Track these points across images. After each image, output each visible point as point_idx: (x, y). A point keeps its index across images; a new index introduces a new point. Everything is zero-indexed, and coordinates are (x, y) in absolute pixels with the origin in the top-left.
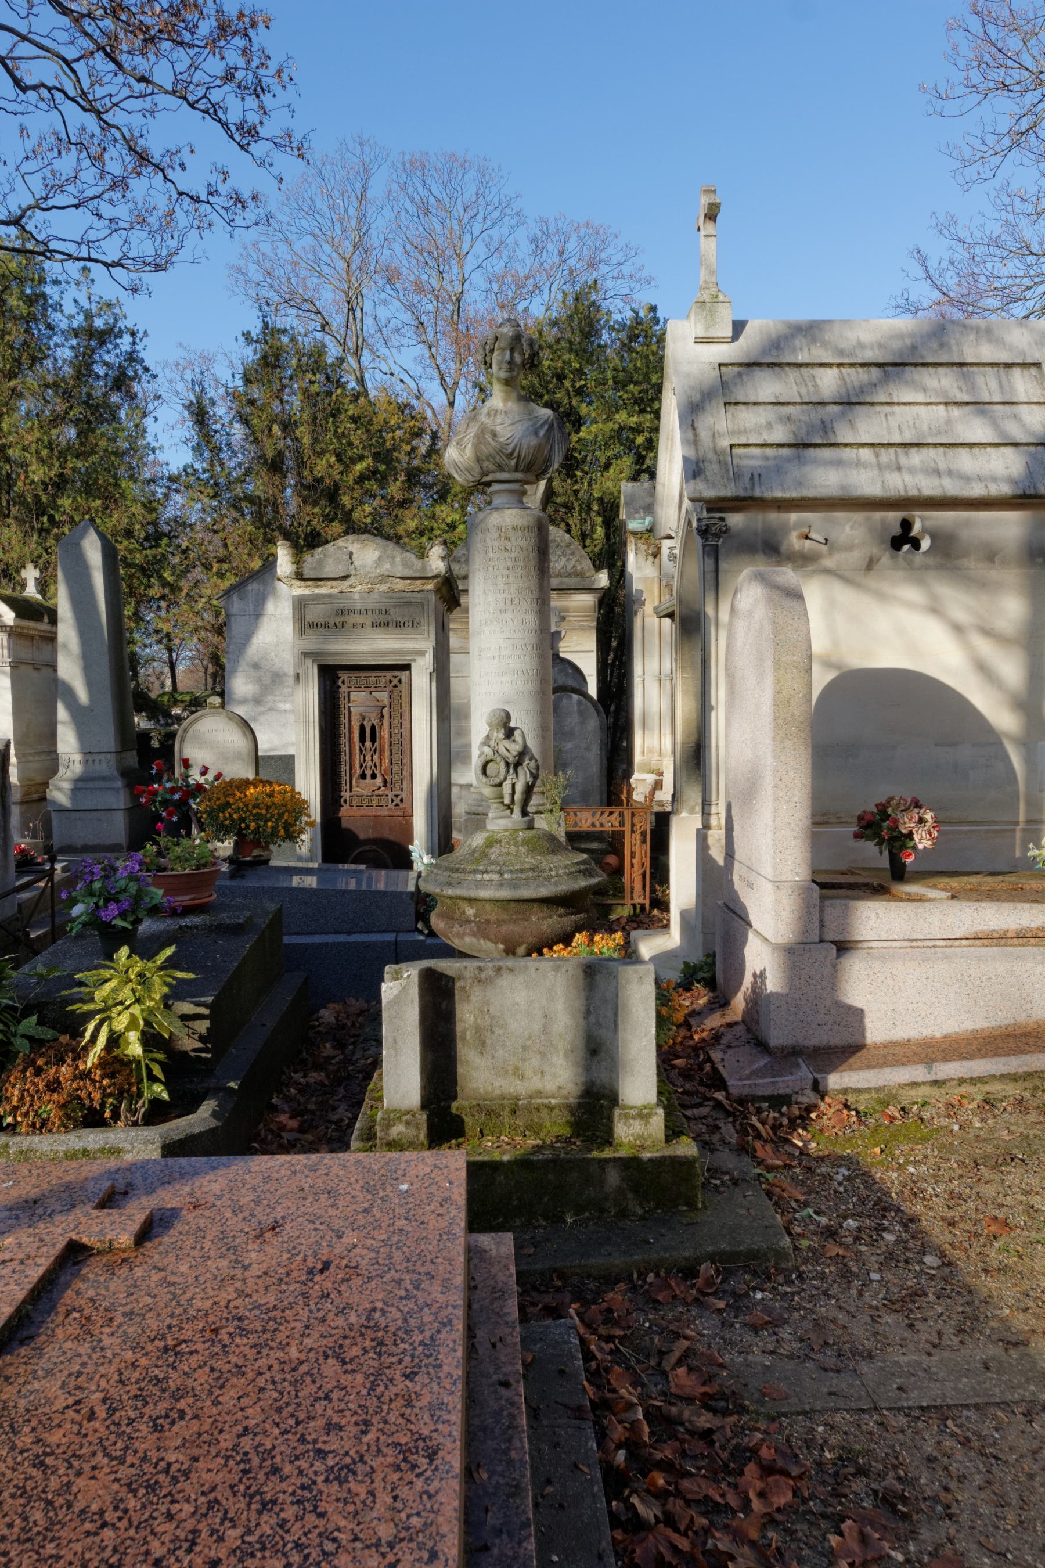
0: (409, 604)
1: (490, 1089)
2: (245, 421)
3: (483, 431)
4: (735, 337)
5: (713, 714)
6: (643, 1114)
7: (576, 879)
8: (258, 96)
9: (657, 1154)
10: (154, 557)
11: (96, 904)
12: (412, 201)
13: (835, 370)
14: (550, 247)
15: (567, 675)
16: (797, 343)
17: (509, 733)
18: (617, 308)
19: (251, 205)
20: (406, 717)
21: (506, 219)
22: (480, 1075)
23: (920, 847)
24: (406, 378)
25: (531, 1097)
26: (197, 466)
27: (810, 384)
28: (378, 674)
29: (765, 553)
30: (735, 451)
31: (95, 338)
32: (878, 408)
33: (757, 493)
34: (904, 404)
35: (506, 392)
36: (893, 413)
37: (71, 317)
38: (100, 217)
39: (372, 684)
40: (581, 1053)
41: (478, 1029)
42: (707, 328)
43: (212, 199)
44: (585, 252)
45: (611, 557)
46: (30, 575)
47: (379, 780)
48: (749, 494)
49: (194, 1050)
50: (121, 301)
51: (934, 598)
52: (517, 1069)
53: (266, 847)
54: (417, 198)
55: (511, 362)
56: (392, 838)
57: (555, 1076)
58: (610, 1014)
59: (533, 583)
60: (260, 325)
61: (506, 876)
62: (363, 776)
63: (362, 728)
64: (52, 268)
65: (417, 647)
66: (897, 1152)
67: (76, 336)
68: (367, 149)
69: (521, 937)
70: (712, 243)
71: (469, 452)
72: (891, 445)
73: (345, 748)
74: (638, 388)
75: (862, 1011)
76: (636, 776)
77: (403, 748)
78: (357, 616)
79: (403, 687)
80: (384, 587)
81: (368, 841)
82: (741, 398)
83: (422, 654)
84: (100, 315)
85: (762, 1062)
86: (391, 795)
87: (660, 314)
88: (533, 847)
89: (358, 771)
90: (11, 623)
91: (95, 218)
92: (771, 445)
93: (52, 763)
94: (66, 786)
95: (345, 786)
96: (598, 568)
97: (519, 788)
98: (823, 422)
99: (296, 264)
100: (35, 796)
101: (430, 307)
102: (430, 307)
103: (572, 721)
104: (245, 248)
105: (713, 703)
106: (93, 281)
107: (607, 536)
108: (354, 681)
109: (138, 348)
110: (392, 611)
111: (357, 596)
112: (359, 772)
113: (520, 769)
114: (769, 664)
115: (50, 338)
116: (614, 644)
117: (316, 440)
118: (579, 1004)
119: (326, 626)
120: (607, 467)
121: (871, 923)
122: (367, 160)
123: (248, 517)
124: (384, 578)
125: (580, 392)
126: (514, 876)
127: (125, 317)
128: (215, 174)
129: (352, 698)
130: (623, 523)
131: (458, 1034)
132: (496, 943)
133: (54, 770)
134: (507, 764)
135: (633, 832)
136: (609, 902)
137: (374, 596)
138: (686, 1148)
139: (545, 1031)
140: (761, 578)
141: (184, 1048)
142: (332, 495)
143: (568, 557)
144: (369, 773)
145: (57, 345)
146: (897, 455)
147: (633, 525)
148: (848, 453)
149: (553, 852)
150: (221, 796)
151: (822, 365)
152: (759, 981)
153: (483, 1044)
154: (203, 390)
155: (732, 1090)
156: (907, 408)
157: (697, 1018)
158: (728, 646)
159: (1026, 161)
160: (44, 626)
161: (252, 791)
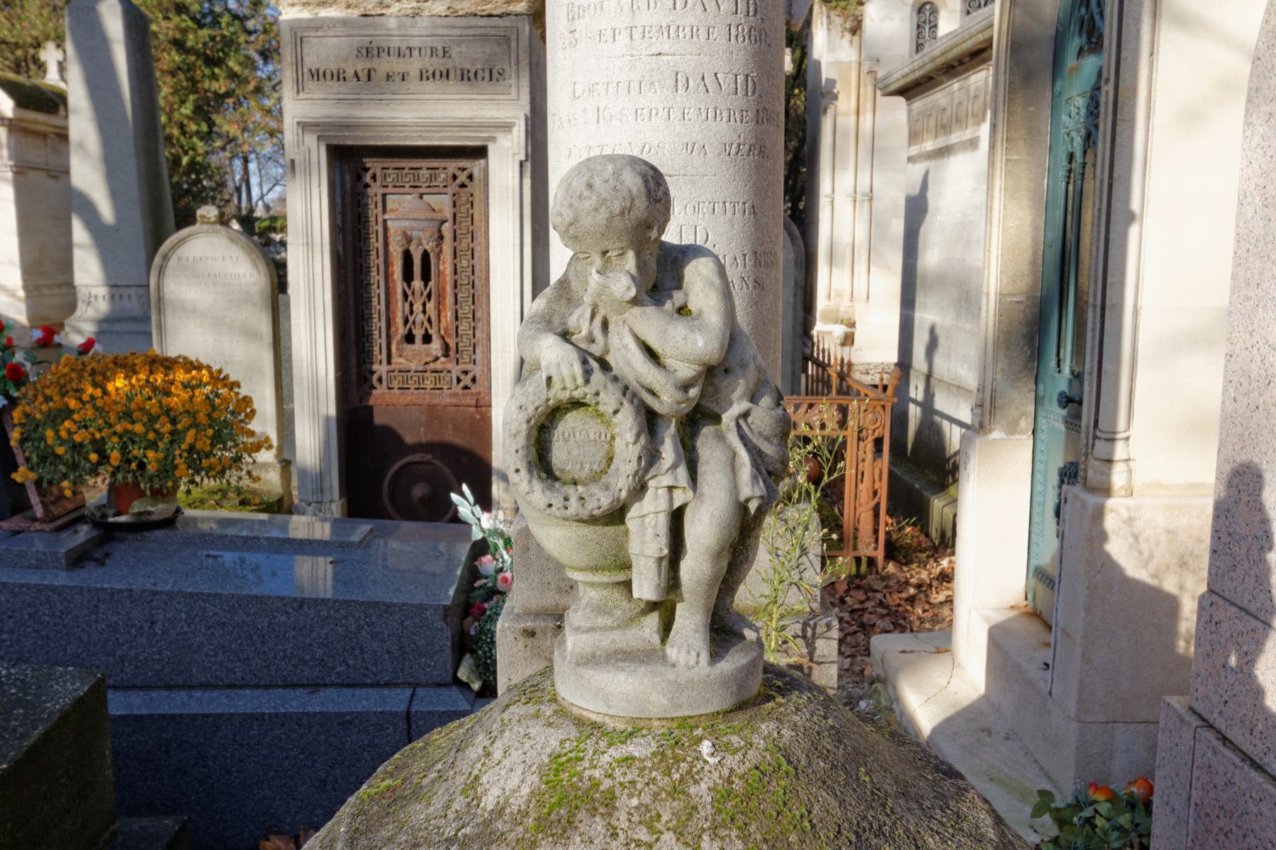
5: (1133, 231)
17: (662, 274)
20: (480, 238)
39: (423, 182)
47: (436, 346)
56: (457, 441)
63: (407, 257)
78: (394, 59)
79: (475, 187)
83: (507, 127)
86: (456, 371)
89: (401, 331)
93: (69, 300)
95: (379, 354)
97: (704, 531)
105: (1135, 205)
110: (454, 52)
111: (392, 23)
119: (339, 76)
129: (390, 205)
133: (71, 307)
134: (650, 421)
137: (423, 23)
161: (120, 382)
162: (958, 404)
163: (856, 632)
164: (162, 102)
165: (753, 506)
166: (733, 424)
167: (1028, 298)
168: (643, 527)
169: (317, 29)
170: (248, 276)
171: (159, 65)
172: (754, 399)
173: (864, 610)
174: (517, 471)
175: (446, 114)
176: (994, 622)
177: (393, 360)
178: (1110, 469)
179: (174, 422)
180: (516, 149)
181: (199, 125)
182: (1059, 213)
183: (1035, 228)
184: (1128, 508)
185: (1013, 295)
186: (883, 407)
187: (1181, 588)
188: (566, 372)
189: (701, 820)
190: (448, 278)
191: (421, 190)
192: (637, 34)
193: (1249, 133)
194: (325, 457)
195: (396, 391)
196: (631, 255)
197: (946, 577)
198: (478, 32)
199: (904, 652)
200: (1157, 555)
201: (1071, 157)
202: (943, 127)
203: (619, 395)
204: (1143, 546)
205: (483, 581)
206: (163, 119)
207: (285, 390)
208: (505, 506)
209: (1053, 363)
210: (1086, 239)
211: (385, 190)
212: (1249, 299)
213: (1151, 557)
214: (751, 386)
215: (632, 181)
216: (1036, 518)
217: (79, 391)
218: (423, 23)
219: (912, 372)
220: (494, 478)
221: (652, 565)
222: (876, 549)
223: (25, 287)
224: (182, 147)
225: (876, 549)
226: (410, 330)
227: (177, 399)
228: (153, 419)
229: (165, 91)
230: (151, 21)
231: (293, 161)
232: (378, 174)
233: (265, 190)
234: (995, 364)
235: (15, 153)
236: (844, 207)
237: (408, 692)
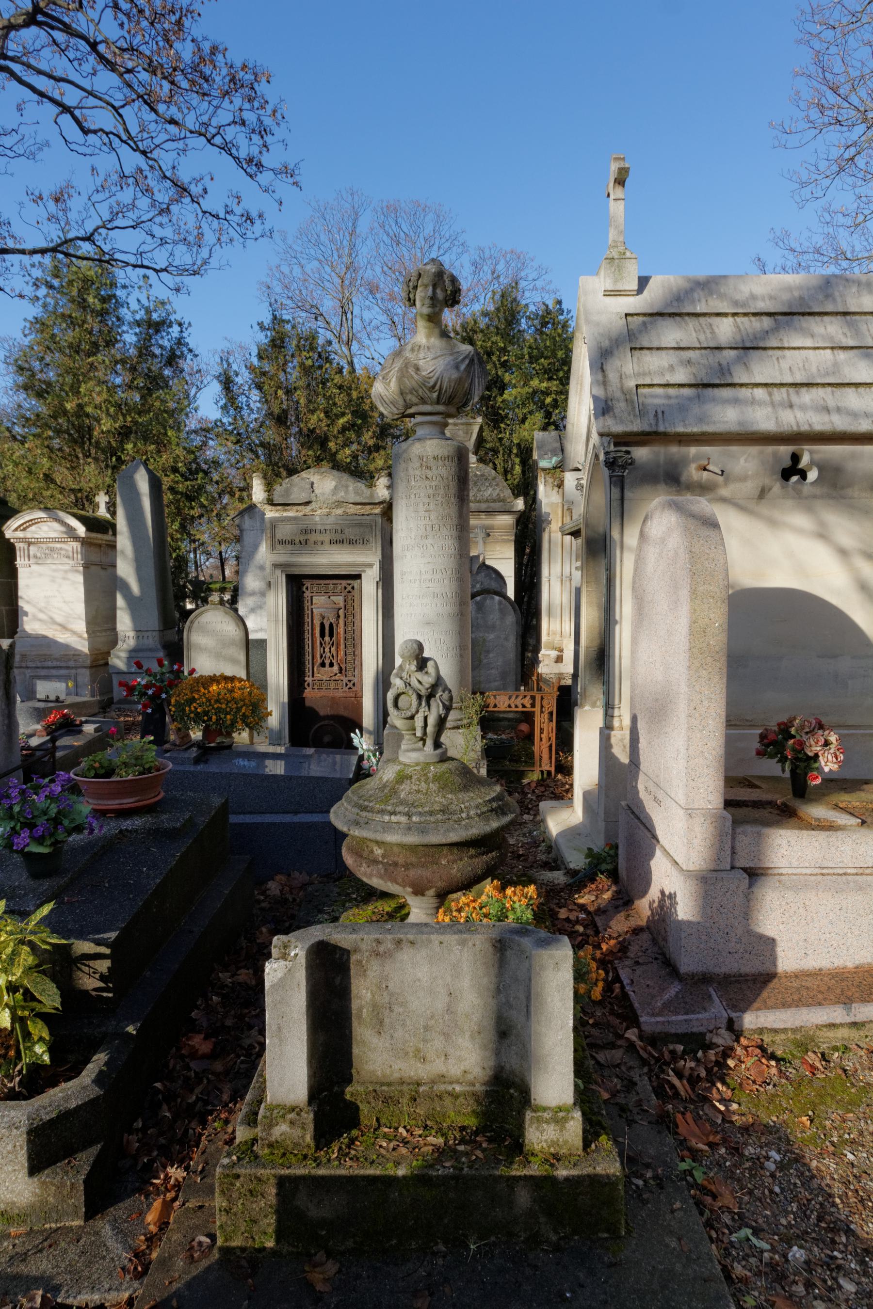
0: (360, 525)
1: (388, 1072)
2: (259, 387)
3: (406, 366)
4: (640, 290)
5: (617, 628)
6: (558, 1116)
7: (487, 819)
8: (262, 137)
9: (575, 1172)
10: (193, 486)
11: (13, 829)
12: (388, 235)
13: (730, 319)
14: (485, 268)
15: (491, 578)
16: (696, 295)
18: (532, 300)
19: (258, 222)
20: (357, 617)
21: (454, 248)
22: (376, 1056)
23: (826, 769)
25: (433, 1082)
26: (225, 420)
27: (708, 331)
29: (666, 484)
30: (641, 391)
31: (154, 326)
32: (770, 352)
33: (661, 429)
34: (794, 348)
35: (429, 328)
36: (784, 357)
37: (134, 312)
38: (153, 236)
40: (490, 1035)
41: (375, 1006)
42: (616, 281)
44: (510, 272)
45: (526, 487)
46: (102, 499)
47: (336, 668)
48: (654, 429)
49: (95, 990)
51: (822, 524)
52: (418, 1050)
53: (229, 735)
54: (391, 233)
55: (433, 298)
57: (460, 1059)
58: (522, 996)
59: (453, 510)
60: (270, 317)
61: (414, 819)
62: (323, 665)
63: (322, 626)
64: (121, 275)
65: (367, 560)
66: (828, 1123)
67: (139, 326)
68: (356, 197)
69: (429, 882)
70: (621, 205)
71: (393, 385)
72: (782, 385)
73: (308, 642)
74: (547, 361)
75: (774, 940)
76: (543, 652)
79: (355, 593)
80: (339, 511)
81: (327, 717)
82: (646, 344)
83: (371, 566)
84: (156, 311)
85: (674, 989)
86: (345, 680)
88: (444, 785)
89: (319, 661)
90: (83, 535)
91: (149, 237)
92: (673, 385)
94: (123, 655)
96: (516, 496)
97: (431, 721)
98: (720, 365)
99: (305, 280)
100: (102, 662)
101: (400, 311)
102: (400, 311)
103: (494, 617)
105: (617, 617)
109: (185, 335)
110: (346, 531)
111: (317, 518)
113: (433, 702)
114: (684, 593)
115: (119, 326)
116: (528, 551)
117: (310, 401)
118: (487, 981)
119: (292, 543)
120: (523, 421)
121: (783, 851)
122: (356, 206)
123: (262, 457)
124: (339, 503)
126: (423, 819)
130: (536, 463)
131: (354, 1012)
132: (404, 887)
133: (114, 643)
134: (420, 697)
135: (542, 712)
136: (522, 768)
137: (332, 519)
138: (609, 1166)
139: (449, 1010)
140: (678, 508)
141: (85, 988)
142: (323, 442)
143: (488, 483)
144: (327, 662)
145: (123, 332)
146: (788, 395)
147: (543, 464)
148: (745, 393)
149: (465, 788)
150: (188, 692)
151: (718, 315)
152: (668, 902)
153: (381, 1022)
154: (229, 364)
155: (645, 1027)
156: (797, 352)
157: (603, 917)
158: (636, 570)
159: (846, 187)
160: (109, 537)
161: (215, 688)
189: (431, 780)
215: (415, 646)
217: (199, 691)
223: (87, 632)
227: (237, 694)
235: (85, 557)
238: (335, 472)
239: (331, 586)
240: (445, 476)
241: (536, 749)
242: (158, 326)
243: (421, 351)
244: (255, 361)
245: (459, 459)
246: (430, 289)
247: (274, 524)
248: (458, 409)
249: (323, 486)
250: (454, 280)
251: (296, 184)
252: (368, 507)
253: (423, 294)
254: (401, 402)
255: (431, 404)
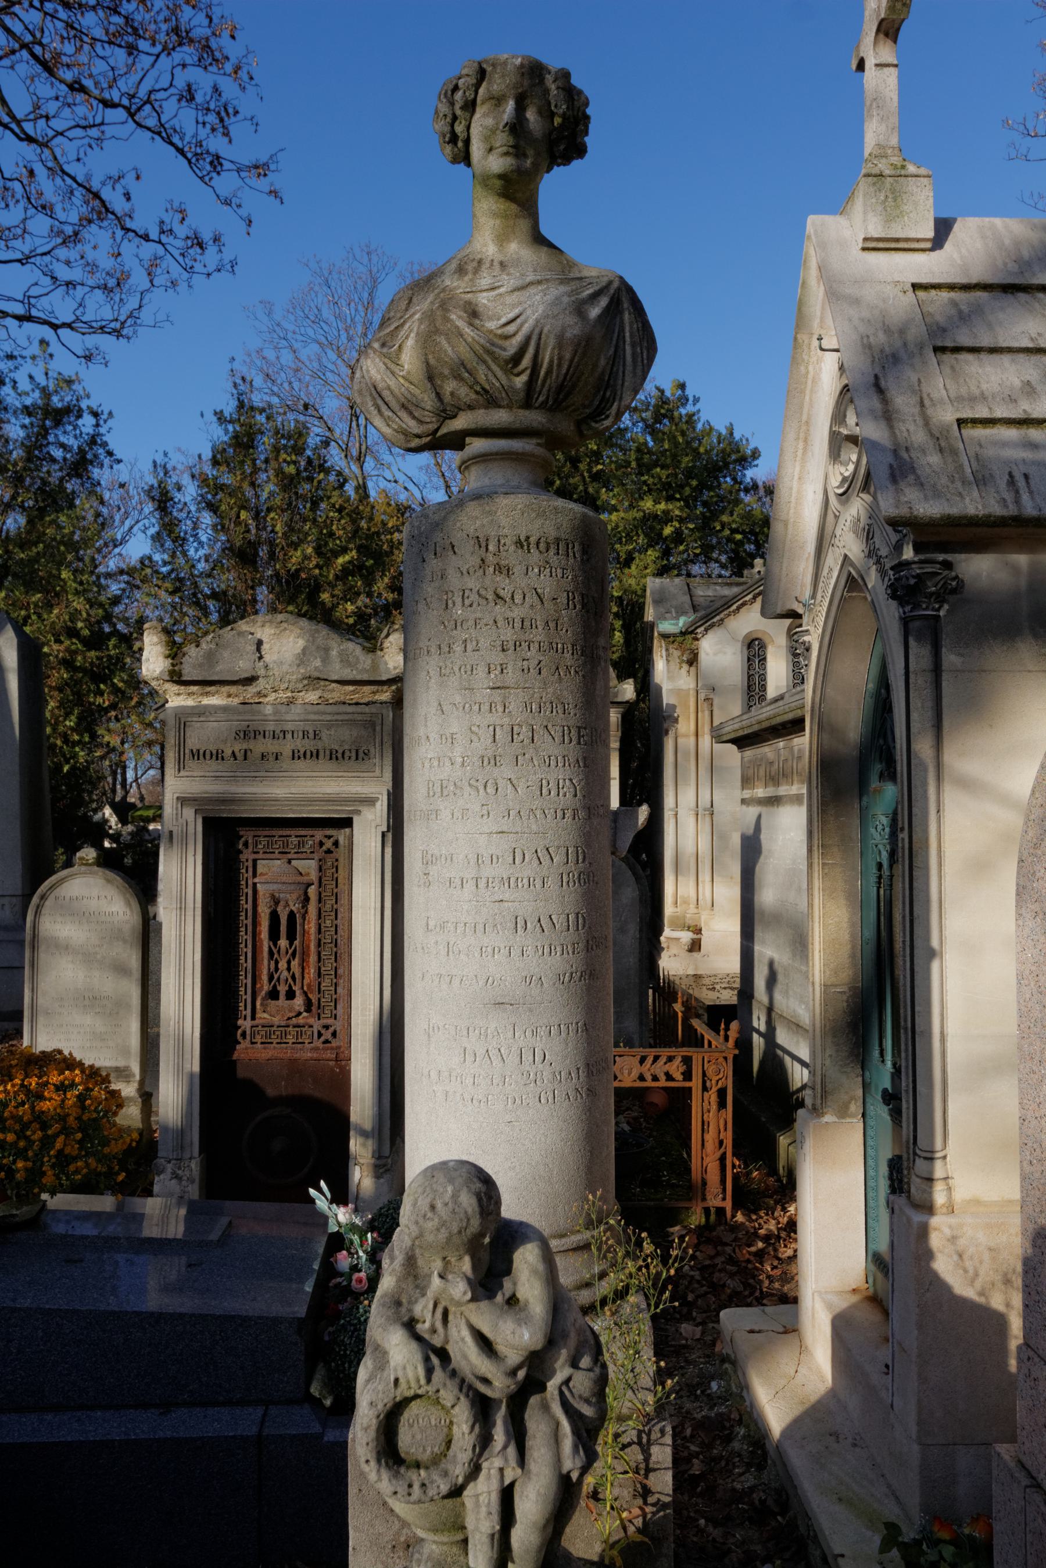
2: (212, 507)
5: (935, 966)
19: (211, 250)
20: (343, 900)
24: (411, 486)
26: (157, 557)
28: (302, 832)
30: (969, 432)
42: (889, 220)
43: (164, 239)
47: (299, 1002)
48: (1012, 510)
50: (81, 376)
55: (517, 128)
56: (317, 1094)
60: (234, 403)
62: (274, 995)
63: (274, 917)
67: (30, 414)
68: (374, 257)
71: (409, 358)
76: (667, 933)
77: (336, 949)
78: (269, 741)
80: (312, 696)
81: (280, 1100)
83: (371, 802)
87: (690, 392)
89: (266, 987)
96: (621, 678)
97: (531, 1506)
104: (249, 355)
105: (935, 943)
106: (51, 355)
107: (627, 642)
108: (264, 841)
109: (102, 430)
110: (325, 734)
111: (268, 710)
112: (266, 987)
117: (292, 530)
120: (628, 562)
122: (375, 270)
125: (596, 477)
127: (88, 396)
128: (171, 213)
129: (259, 870)
134: (483, 1408)
135: (705, 1089)
137: (297, 710)
144: (282, 989)
162: (798, 1042)
163: (706, 1293)
164: (48, 715)
165: (575, 1476)
166: (556, 1392)
167: (850, 989)
168: (477, 1504)
169: (199, 715)
170: (121, 913)
171: (49, 682)
172: (574, 1364)
173: (715, 1266)
174: (367, 1461)
175: (315, 790)
176: (838, 1310)
177: (258, 1016)
178: (931, 1187)
179: (44, 1127)
180: (378, 821)
181: (82, 735)
182: (873, 914)
183: (852, 925)
184: (950, 1227)
185: (836, 986)
186: (725, 1058)
187: (1008, 1305)
188: (411, 1375)
190: (313, 937)
191: (290, 856)
192: (482, 884)
193: (1021, 923)
194: (188, 1114)
195: (259, 1045)
196: (467, 1259)
197: (792, 1226)
198: (346, 717)
199: (752, 1332)
200: (982, 1272)
201: (880, 866)
202: (772, 779)
203: (456, 1391)
204: (968, 1264)
205: (339, 1280)
206: (48, 730)
207: (150, 1015)
208: (361, 1161)
209: (876, 1053)
210: (898, 945)
211: (256, 856)
212: (1034, 1073)
213: (976, 1275)
214: (572, 1352)
215: (468, 1202)
216: (871, 1203)
218: (297, 710)
219: (754, 1003)
220: (352, 1133)
221: (486, 1540)
222: (724, 1199)
224: (64, 756)
225: (724, 1199)
226: (275, 986)
228: (26, 1126)
229: (52, 704)
230: (43, 644)
231: (171, 832)
232: (248, 1032)
233: (140, 773)
234: (824, 1050)
236: (688, 822)
237: (260, 1411)
238: (304, 623)
239: (294, 840)
240: (547, 592)
241: (695, 1164)
242: (59, 416)
243: (484, 272)
244: (209, 470)
245: (584, 551)
246: (510, 105)
247: (184, 719)
248: (579, 424)
249: (281, 644)
250: (572, 94)
251: (274, 193)
252: (367, 689)
253: (490, 121)
254: (428, 401)
255: (509, 407)
